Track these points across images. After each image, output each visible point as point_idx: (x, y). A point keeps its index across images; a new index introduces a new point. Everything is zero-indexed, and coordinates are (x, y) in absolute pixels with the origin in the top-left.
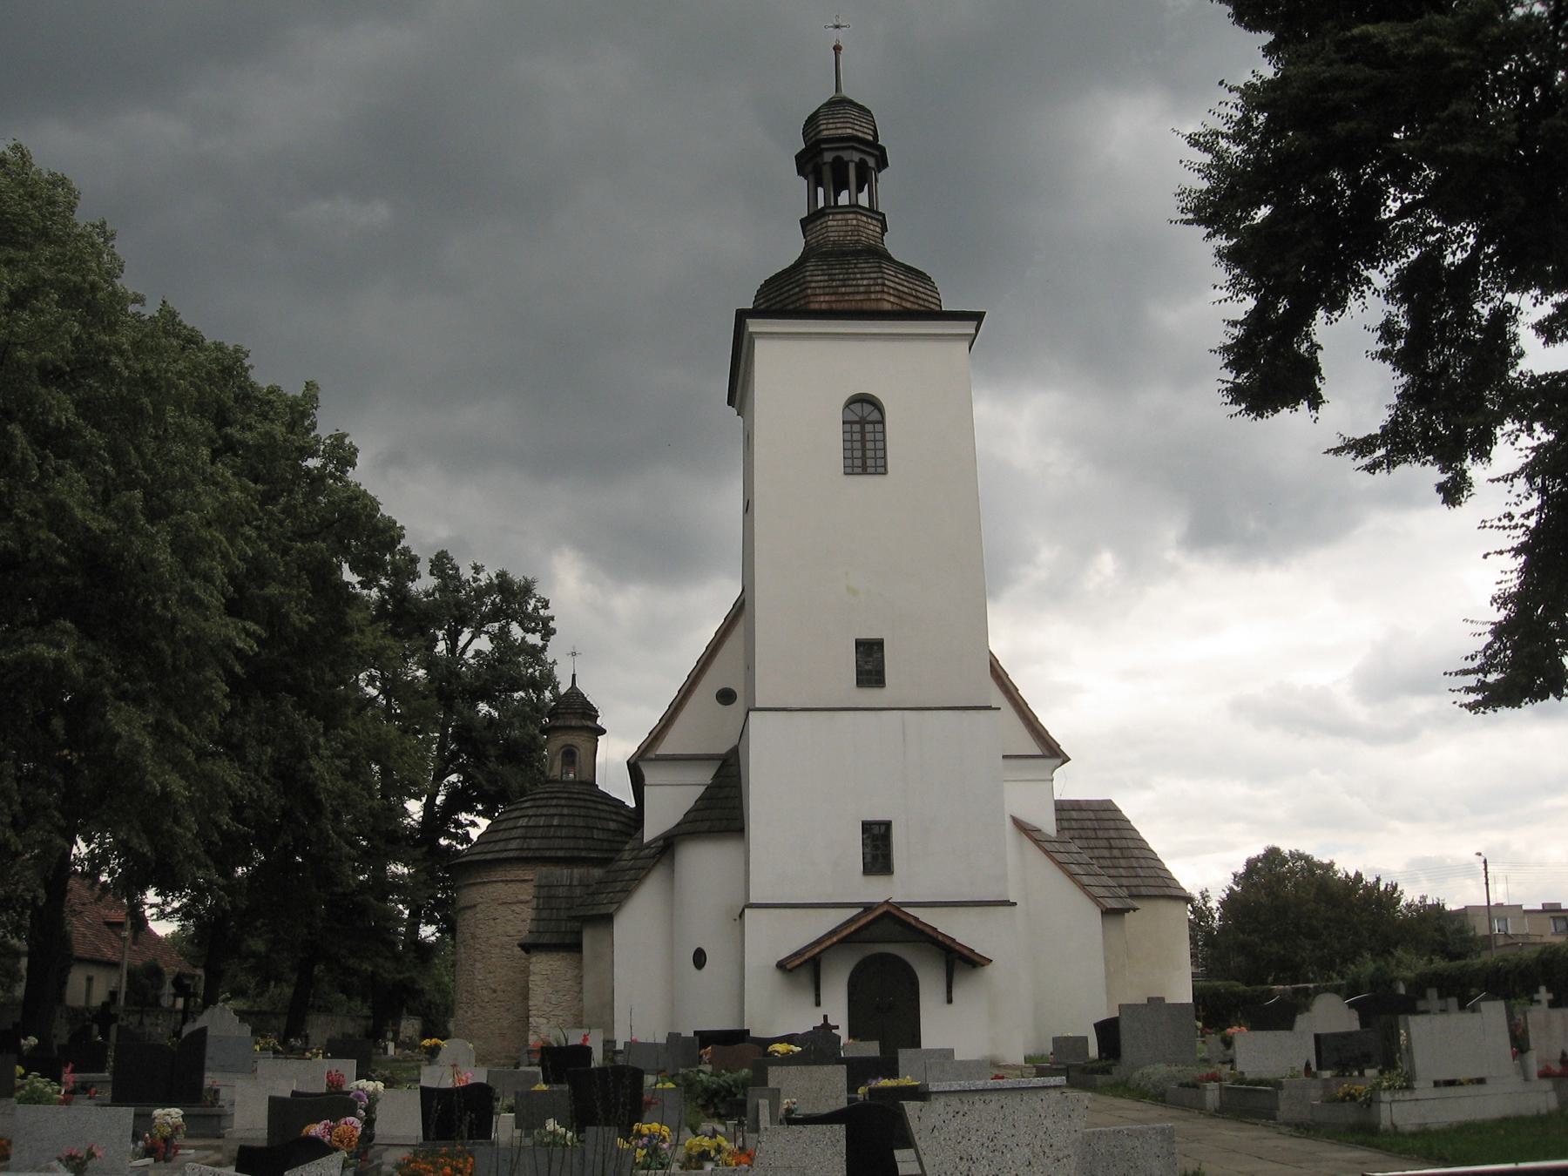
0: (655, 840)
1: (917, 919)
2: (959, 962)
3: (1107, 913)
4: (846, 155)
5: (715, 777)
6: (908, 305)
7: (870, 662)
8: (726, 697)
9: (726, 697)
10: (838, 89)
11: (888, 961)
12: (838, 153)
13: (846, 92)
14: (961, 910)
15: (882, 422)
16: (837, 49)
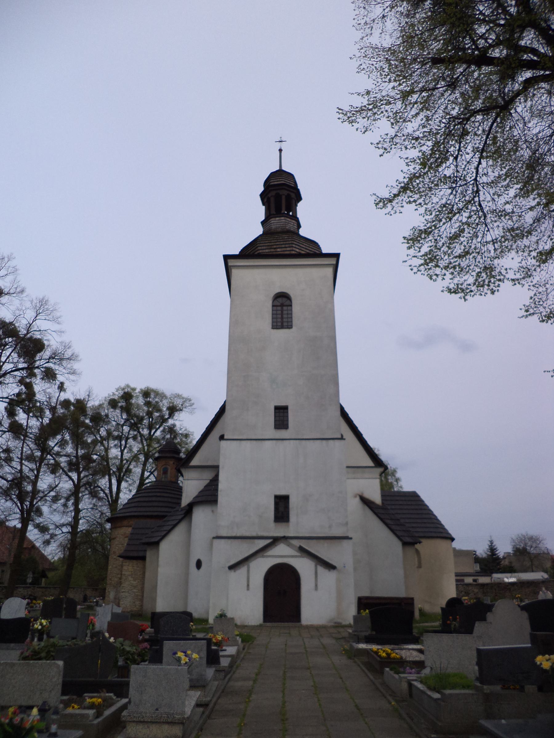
0: (185, 507)
3: (405, 544)
7: (281, 415)
12: (281, 194)
13: (284, 168)
15: (291, 306)
16: (280, 150)
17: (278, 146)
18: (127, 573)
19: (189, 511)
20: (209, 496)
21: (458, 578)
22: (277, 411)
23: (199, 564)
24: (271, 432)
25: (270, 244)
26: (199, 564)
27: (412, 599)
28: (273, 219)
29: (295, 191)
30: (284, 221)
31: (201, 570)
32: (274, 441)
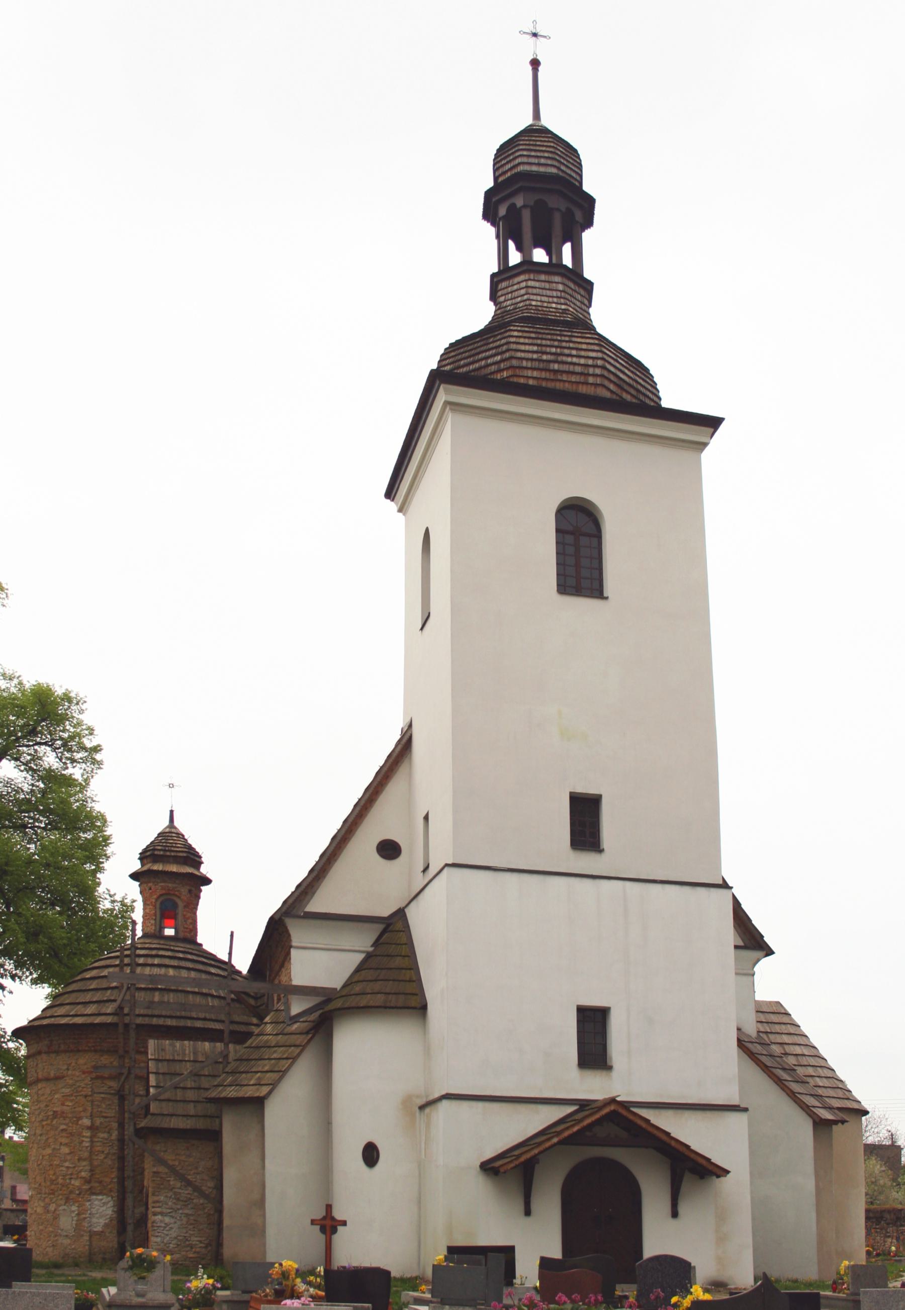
1: (647, 1121)
2: (691, 1171)
5: (376, 944)
6: (628, 398)
7: (585, 819)
8: (389, 850)
9: (389, 850)
11: (602, 1165)
12: (539, 195)
13: (546, 121)
14: (687, 1114)
17: (529, 49)
21: (762, 1018)
23: (371, 1154)
26: (371, 1154)
27: (600, 796)
30: (561, 287)
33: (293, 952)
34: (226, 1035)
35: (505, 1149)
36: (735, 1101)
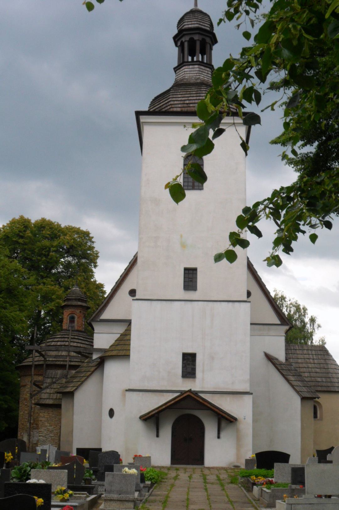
2: (225, 420)
4: (196, 37)
7: (190, 277)
10: (196, 4)
13: (200, 7)
18: (43, 419)
19: (101, 363)
20: (121, 350)
22: (187, 272)
23: (111, 413)
24: (181, 294)
25: (183, 99)
26: (111, 413)
28: (186, 67)
29: (211, 36)
30: (198, 69)
31: (114, 418)
32: (183, 302)
33: (95, 335)
34: (67, 366)
35: (228, 412)
36: (248, 390)
